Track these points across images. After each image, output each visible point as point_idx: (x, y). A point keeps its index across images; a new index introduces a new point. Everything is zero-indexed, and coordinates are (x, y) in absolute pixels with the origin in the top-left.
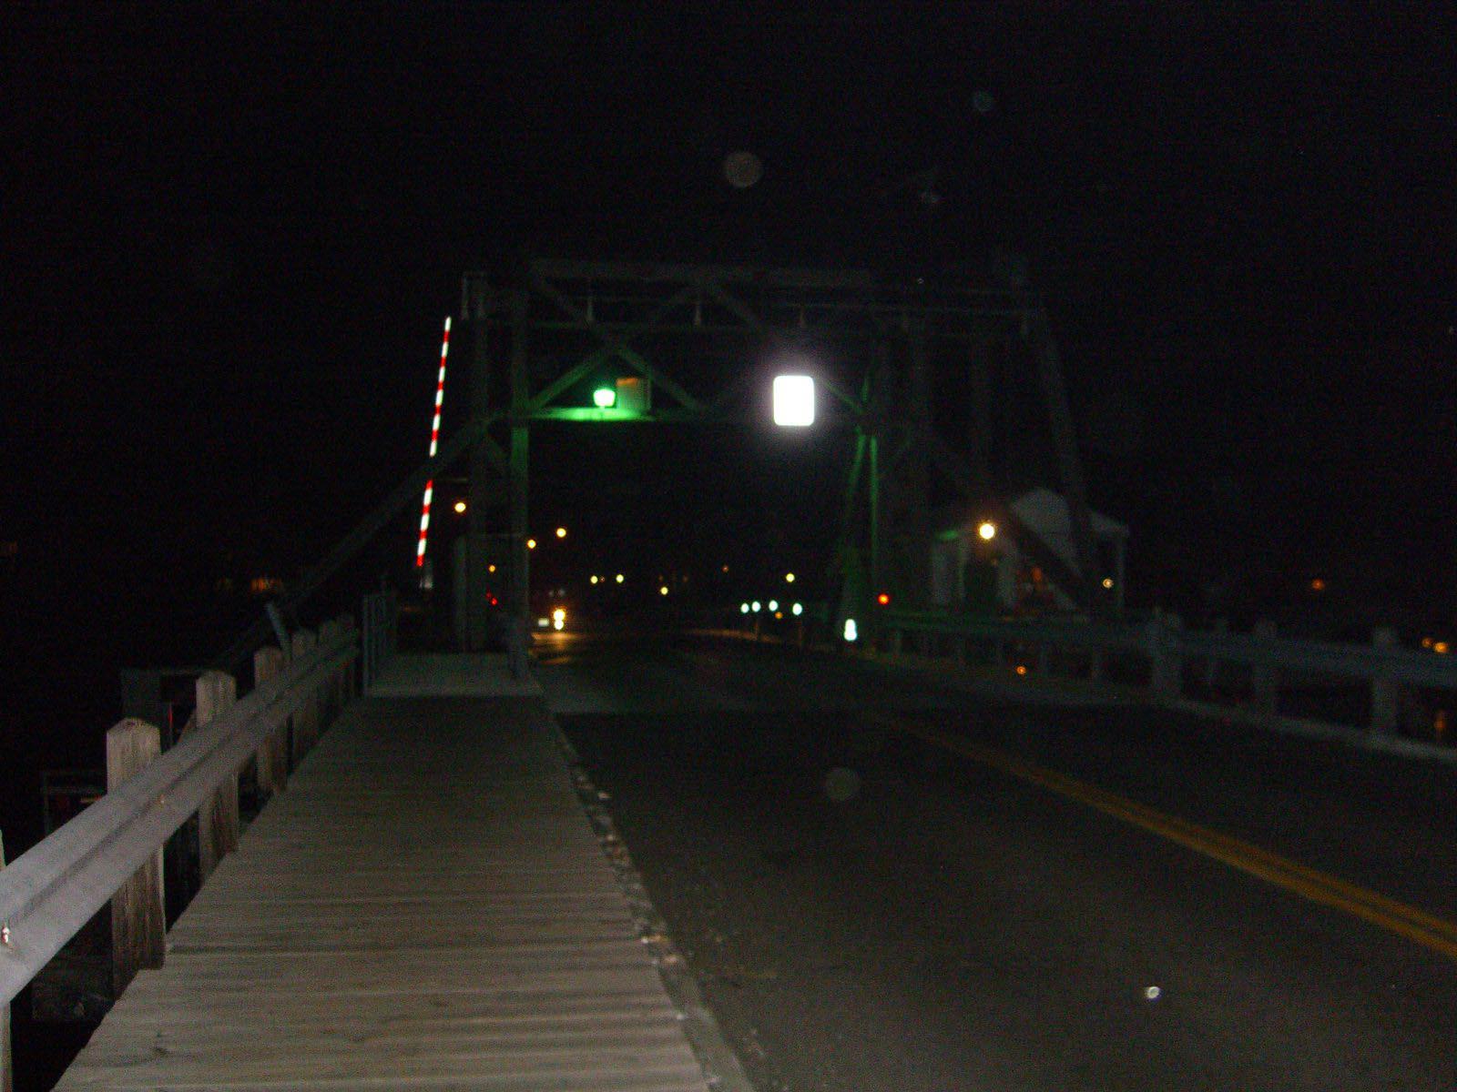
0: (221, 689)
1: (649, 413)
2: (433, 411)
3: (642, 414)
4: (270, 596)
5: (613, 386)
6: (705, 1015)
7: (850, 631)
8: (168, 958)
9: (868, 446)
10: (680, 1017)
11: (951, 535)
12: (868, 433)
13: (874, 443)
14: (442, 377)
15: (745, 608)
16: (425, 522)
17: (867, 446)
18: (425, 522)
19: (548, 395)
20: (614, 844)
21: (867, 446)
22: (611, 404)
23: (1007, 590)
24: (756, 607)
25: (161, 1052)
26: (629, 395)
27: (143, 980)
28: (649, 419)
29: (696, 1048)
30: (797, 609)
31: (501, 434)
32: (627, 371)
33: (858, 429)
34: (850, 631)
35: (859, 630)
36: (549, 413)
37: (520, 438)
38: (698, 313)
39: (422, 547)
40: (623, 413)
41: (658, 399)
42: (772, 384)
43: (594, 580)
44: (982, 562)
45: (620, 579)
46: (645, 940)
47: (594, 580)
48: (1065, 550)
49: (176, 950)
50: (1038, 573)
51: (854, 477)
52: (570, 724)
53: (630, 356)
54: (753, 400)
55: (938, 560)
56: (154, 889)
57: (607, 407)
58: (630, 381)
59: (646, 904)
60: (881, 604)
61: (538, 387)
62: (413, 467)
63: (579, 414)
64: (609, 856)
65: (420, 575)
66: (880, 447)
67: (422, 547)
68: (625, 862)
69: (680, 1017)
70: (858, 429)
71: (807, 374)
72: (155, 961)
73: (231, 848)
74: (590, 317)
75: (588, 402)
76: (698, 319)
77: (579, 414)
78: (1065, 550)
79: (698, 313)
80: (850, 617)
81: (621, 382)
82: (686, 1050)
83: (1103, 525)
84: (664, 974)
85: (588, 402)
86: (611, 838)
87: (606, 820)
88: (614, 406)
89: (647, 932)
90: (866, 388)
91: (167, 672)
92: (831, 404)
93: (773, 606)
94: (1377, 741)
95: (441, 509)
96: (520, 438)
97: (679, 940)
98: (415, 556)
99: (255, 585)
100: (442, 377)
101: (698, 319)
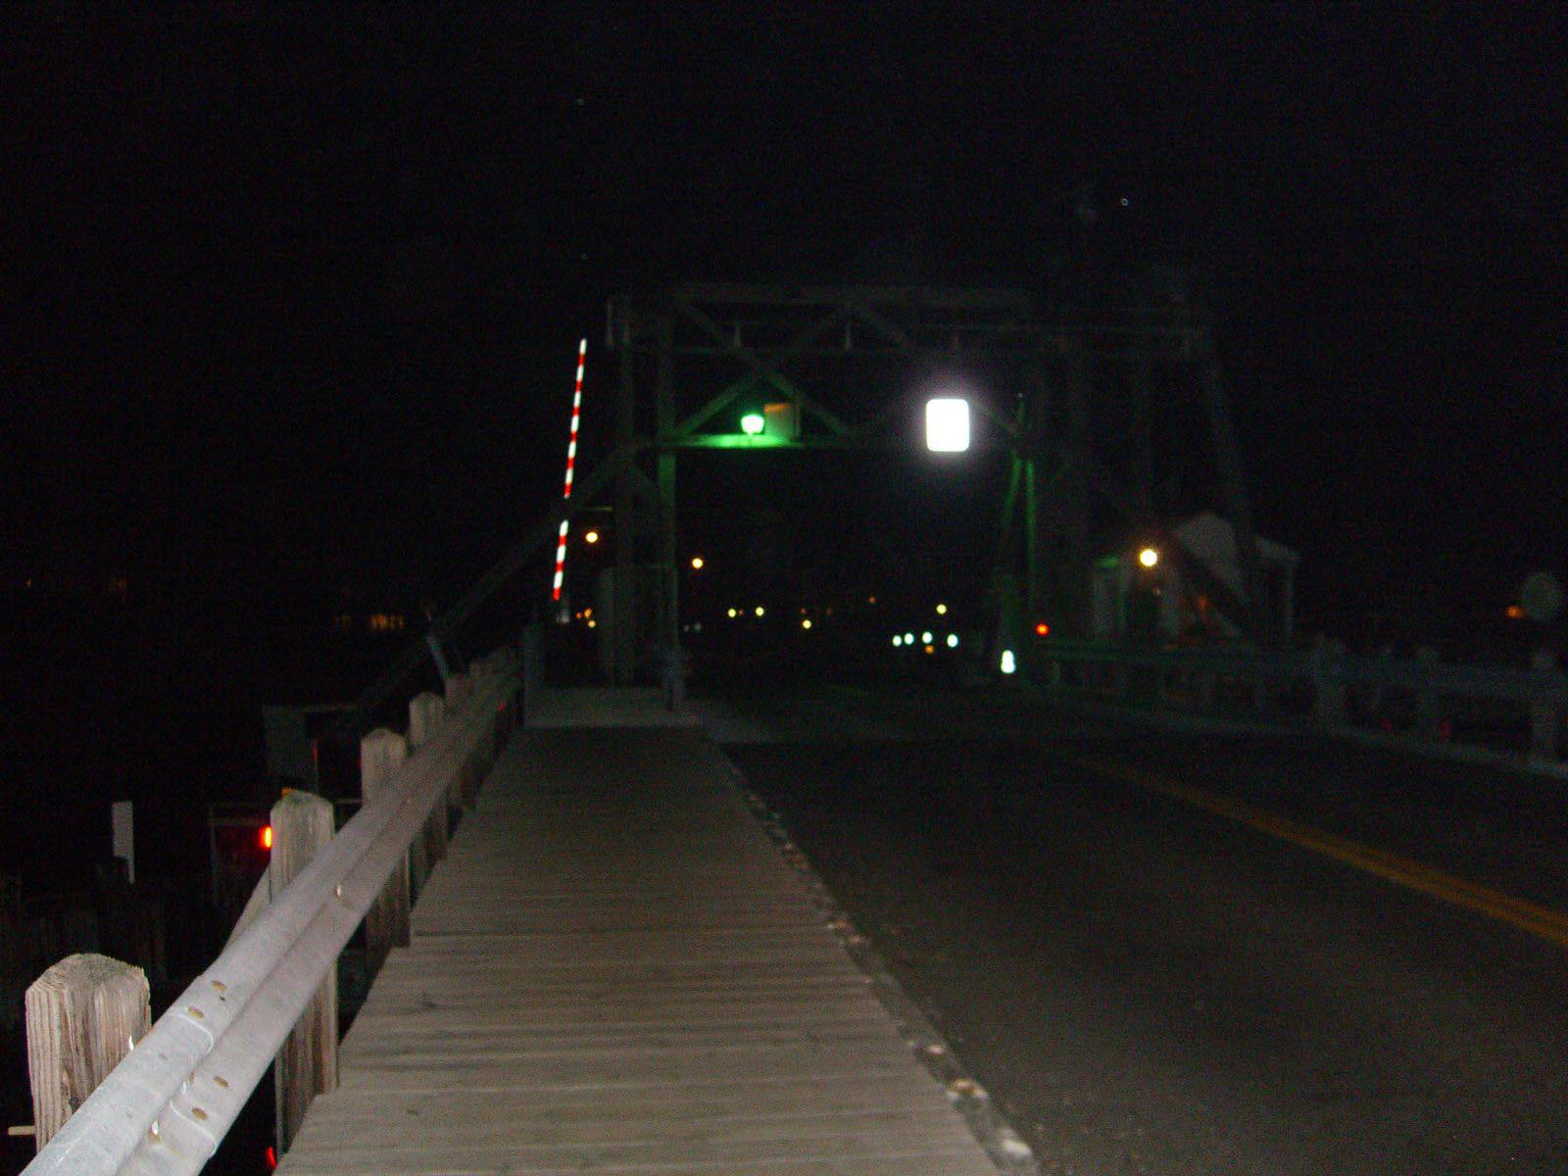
0: (432, 711)
1: (796, 439)
2: (569, 437)
3: (791, 440)
4: (573, 616)
5: (761, 412)
6: (888, 979)
7: (1008, 663)
8: (413, 940)
9: (1025, 471)
10: (868, 981)
11: (1111, 562)
12: (1024, 457)
13: (1030, 469)
14: (577, 402)
15: (897, 641)
16: (561, 553)
17: (1023, 472)
18: (561, 553)
19: (697, 421)
20: (791, 852)
21: (1023, 472)
22: (760, 430)
23: (1171, 619)
24: (909, 639)
25: (432, 1006)
26: (773, 421)
27: (395, 956)
28: (799, 445)
29: (883, 1001)
30: (952, 641)
31: (647, 462)
32: (777, 397)
33: (1014, 452)
34: (1008, 663)
35: (1017, 662)
36: (696, 440)
37: (667, 466)
38: (848, 335)
39: (558, 579)
40: (772, 441)
41: (807, 425)
42: (971, 444)
43: (732, 613)
44: (1144, 589)
45: (760, 611)
46: (831, 926)
47: (732, 613)
48: (1230, 575)
49: (419, 934)
50: (1202, 602)
51: (1010, 500)
52: (732, 751)
53: (787, 389)
54: (908, 425)
55: (1098, 586)
56: (402, 876)
57: (755, 434)
58: (777, 407)
59: (827, 899)
60: (1039, 636)
61: (685, 412)
62: (546, 501)
63: (727, 441)
64: (790, 862)
65: (557, 608)
66: (1036, 473)
67: (558, 579)
68: (805, 866)
69: (867, 981)
70: (1014, 452)
71: (962, 397)
72: (403, 941)
73: (442, 855)
74: (737, 342)
75: (736, 429)
76: (848, 344)
77: (727, 441)
78: (1230, 575)
79: (848, 335)
80: (1007, 649)
81: (769, 408)
82: (876, 1003)
83: (1269, 549)
84: (850, 949)
85: (736, 429)
86: (789, 846)
87: (781, 833)
88: (763, 433)
89: (832, 920)
90: (1021, 412)
91: (307, 709)
92: (987, 429)
93: (927, 638)
94: (1537, 764)
95: (575, 540)
96: (667, 466)
97: (859, 925)
98: (552, 589)
99: (374, 622)
100: (577, 402)
101: (848, 344)
